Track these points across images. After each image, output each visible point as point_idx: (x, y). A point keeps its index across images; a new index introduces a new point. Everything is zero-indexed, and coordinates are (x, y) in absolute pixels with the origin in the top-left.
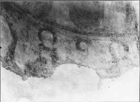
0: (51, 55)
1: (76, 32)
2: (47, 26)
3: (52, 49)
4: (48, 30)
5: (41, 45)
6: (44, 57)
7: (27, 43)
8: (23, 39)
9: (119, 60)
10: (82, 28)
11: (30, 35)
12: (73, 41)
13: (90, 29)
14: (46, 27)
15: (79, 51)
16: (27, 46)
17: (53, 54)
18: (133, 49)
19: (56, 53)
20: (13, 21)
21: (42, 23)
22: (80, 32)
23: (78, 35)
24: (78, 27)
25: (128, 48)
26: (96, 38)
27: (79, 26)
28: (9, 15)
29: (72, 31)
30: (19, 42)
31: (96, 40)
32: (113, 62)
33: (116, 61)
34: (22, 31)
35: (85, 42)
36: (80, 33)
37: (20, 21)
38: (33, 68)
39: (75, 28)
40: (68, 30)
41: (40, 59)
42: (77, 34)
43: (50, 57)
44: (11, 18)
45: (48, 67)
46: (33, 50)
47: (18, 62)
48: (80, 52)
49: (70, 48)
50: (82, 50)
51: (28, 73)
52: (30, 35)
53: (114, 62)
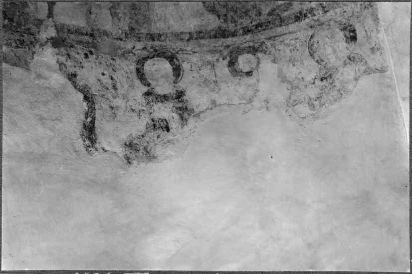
0: (177, 108)
1: (222, 33)
2: (152, 48)
3: (175, 95)
4: (158, 56)
5: (148, 94)
6: (160, 119)
7: (117, 100)
8: (106, 97)
9: (336, 69)
10: (236, 19)
11: (120, 82)
12: (221, 60)
13: (256, 15)
14: (152, 50)
15: (239, 77)
16: (117, 107)
17: (180, 105)
18: (366, 31)
19: (186, 100)
20: (75, 67)
21: (139, 46)
22: (235, 31)
23: (229, 41)
24: (226, 21)
25: (354, 31)
26: (274, 34)
27: (229, 16)
28: (63, 59)
29: (215, 37)
30: (99, 104)
31: (275, 37)
32: (322, 80)
33: (328, 74)
34: (99, 80)
35: (248, 52)
36: (234, 34)
37: (90, 61)
38: (141, 148)
39: (220, 28)
40: (203, 38)
41: (154, 125)
42: (228, 39)
43: (174, 115)
44: (69, 63)
45: (174, 136)
46: (133, 110)
47: (107, 145)
48: (240, 79)
49: (217, 79)
50: (245, 75)
51: (180, 87)
52: (120, 82)
53: (325, 78)
